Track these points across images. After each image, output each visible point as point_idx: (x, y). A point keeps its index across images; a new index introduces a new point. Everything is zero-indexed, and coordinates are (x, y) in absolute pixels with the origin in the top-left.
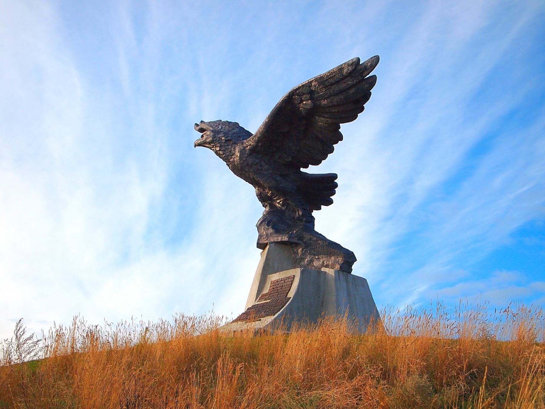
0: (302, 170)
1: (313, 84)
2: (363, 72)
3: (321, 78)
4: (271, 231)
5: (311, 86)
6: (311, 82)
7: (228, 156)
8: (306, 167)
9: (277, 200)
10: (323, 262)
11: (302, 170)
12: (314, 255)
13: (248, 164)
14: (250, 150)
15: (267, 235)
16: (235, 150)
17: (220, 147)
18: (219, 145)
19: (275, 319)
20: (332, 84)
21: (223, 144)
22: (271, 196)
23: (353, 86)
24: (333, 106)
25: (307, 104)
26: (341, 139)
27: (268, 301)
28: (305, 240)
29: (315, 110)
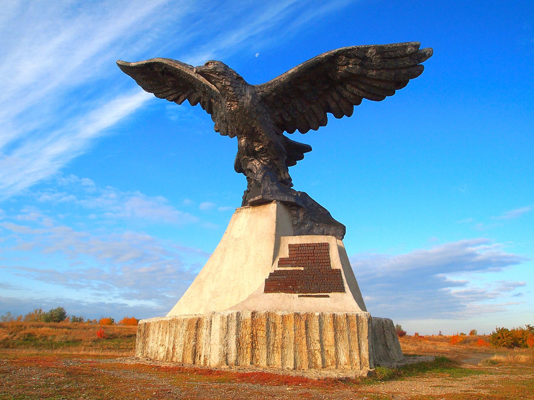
0: (285, 133)
1: (370, 51)
2: (421, 57)
3: (382, 48)
4: (275, 188)
5: (367, 52)
6: (368, 48)
7: (237, 95)
8: (291, 132)
9: (264, 156)
10: (323, 231)
11: (285, 133)
12: (315, 222)
13: (257, 110)
14: (261, 96)
15: (272, 191)
16: (245, 91)
17: (231, 82)
18: (230, 80)
19: (329, 293)
20: (390, 58)
21: (233, 80)
22: (259, 152)
23: (408, 67)
24: (380, 80)
25: (351, 67)
26: (349, 116)
27: (302, 269)
28: (308, 205)
29: (350, 78)
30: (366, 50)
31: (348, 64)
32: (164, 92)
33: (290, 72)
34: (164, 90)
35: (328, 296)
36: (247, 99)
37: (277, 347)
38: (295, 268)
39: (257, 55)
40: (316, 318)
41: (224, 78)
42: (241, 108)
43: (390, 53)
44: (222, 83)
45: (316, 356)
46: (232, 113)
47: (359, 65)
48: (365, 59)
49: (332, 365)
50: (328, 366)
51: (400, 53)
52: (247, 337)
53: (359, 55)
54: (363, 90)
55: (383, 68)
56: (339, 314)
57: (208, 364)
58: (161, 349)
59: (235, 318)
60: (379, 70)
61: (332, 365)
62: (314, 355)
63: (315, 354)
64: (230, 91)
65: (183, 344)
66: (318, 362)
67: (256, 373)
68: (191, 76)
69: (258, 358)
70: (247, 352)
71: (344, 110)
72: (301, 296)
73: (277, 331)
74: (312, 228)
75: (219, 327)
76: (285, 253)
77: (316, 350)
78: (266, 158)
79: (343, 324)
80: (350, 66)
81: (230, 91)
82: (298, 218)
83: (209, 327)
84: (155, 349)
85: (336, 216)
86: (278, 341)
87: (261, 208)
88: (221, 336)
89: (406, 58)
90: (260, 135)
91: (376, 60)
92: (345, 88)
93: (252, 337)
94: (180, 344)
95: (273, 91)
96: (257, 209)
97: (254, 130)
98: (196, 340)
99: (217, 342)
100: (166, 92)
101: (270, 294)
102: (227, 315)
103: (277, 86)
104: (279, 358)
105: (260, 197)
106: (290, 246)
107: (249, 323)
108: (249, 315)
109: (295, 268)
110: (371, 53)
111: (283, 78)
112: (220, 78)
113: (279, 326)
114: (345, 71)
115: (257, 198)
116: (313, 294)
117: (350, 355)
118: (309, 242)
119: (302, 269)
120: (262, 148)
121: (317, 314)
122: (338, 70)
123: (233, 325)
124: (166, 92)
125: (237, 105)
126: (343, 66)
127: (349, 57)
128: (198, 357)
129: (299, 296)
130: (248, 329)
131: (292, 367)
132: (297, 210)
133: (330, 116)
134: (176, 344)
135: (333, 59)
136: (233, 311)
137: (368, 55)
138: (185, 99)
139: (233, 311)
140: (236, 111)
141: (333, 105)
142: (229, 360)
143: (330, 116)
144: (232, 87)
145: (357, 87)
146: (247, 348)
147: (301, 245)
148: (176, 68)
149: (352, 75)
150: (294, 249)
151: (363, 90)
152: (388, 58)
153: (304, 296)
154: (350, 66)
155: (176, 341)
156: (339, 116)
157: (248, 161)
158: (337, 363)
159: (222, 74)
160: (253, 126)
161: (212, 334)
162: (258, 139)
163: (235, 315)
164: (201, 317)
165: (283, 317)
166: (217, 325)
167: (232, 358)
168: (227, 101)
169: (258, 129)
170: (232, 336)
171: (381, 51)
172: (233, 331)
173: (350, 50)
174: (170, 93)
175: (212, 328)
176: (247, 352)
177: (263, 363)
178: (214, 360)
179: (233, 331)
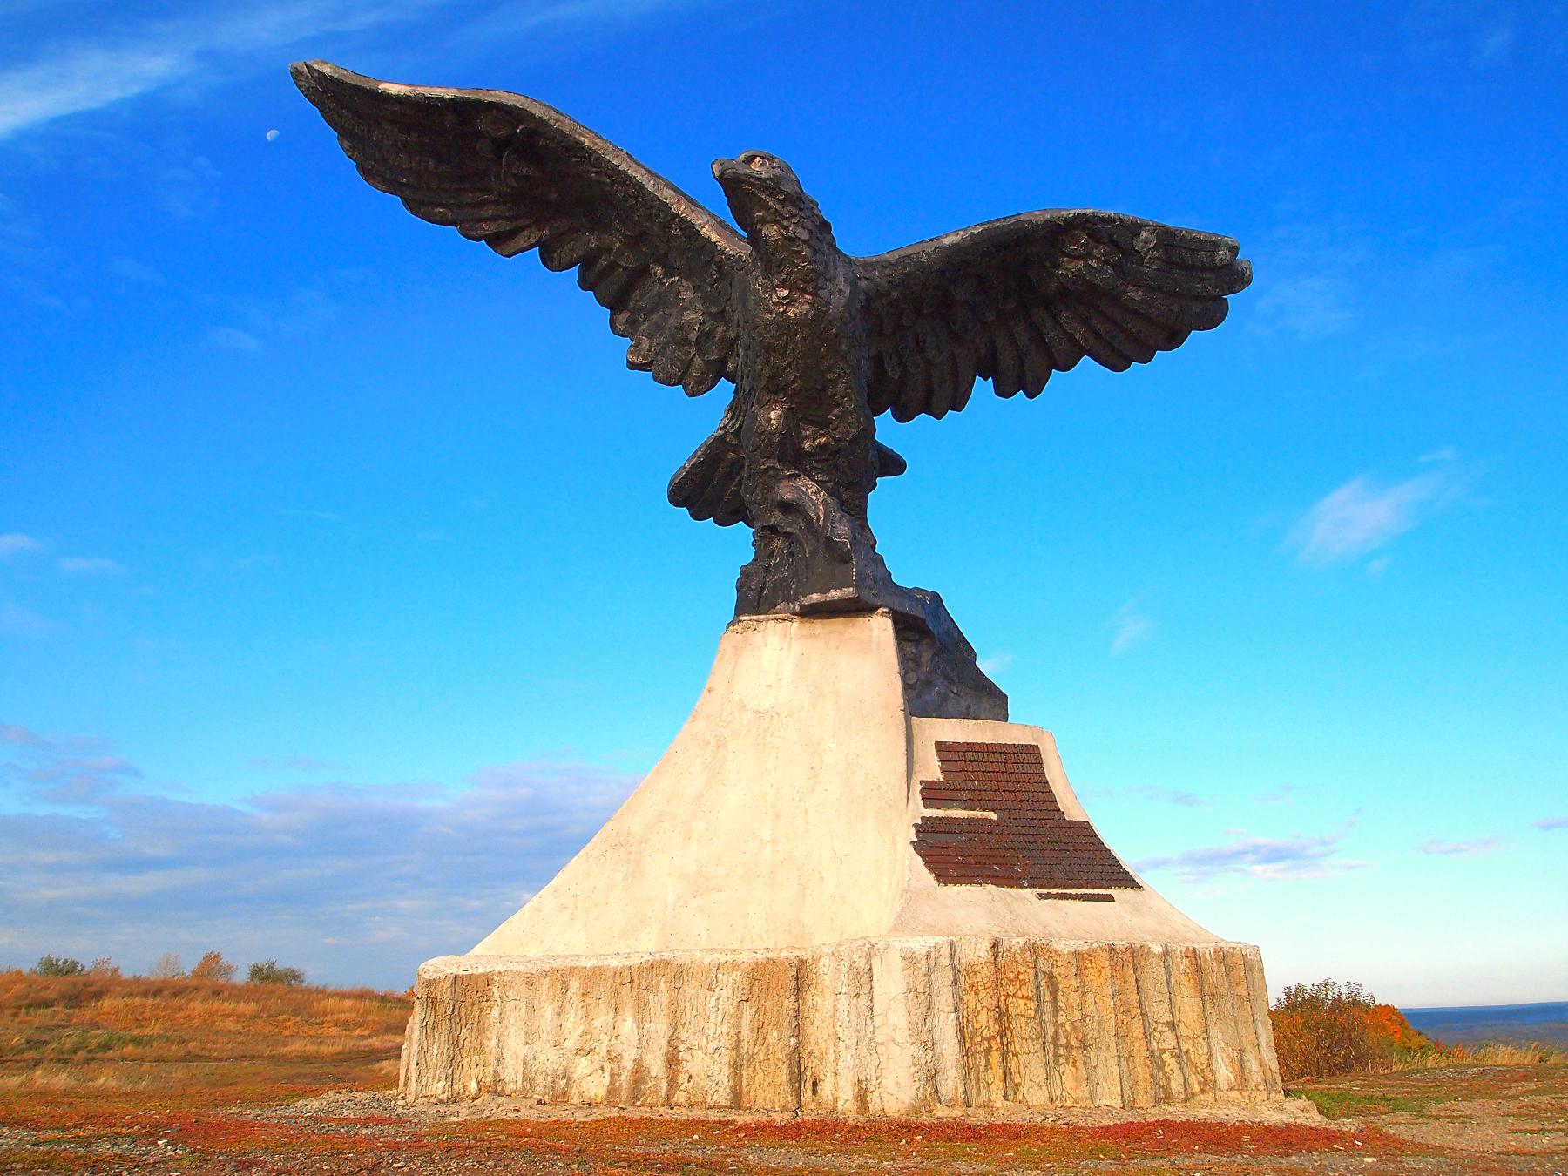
1: (1144, 234)
9: (822, 471)
22: (810, 455)
25: (1091, 265)
26: (1031, 395)
27: (993, 816)
29: (1084, 295)
30: (1135, 228)
31: (1089, 255)
32: (459, 206)
33: (946, 241)
34: (468, 197)
35: (1110, 898)
36: (838, 296)
37: (1068, 1046)
38: (972, 814)
39: (271, 135)
40: (1155, 960)
41: (793, 216)
42: (820, 316)
43: (1185, 253)
44: (786, 228)
45: (1167, 1069)
46: (783, 324)
47: (1114, 266)
48: (1130, 252)
49: (1203, 1091)
50: (1193, 1094)
51: (1204, 257)
52: (983, 1017)
53: (1112, 235)
54: (1097, 334)
55: (1160, 288)
56: (1201, 948)
57: (875, 1107)
58: (583, 1066)
59: (947, 961)
60: (1152, 289)
61: (1203, 1091)
62: (1161, 1065)
63: (1164, 1062)
64: (804, 259)
65: (726, 1042)
66: (1173, 1084)
67: (660, 1123)
68: (631, 178)
69: (1017, 1080)
70: (988, 1063)
71: (1021, 379)
72: (1047, 896)
73: (1060, 997)
74: (945, 698)
75: (903, 989)
76: (932, 769)
77: (1163, 1051)
78: (826, 478)
79: (1215, 976)
80: (1093, 263)
81: (804, 259)
82: (918, 664)
83: (866, 989)
84: (548, 1059)
85: (986, 665)
86: (1068, 1027)
87: (838, 624)
88: (914, 1018)
89: (1209, 275)
90: (838, 405)
91: (1151, 264)
92: (1055, 317)
93: (998, 1020)
94: (715, 1044)
95: (894, 286)
96: (819, 626)
97: (823, 389)
98: (798, 1030)
99: (902, 1034)
100: (472, 205)
101: (964, 887)
102: (924, 951)
103: (908, 275)
104: (1076, 1079)
105: (849, 592)
106: (941, 748)
107: (985, 975)
108: (982, 951)
109: (972, 814)
110: (1146, 242)
111: (928, 254)
112: (784, 211)
113: (1067, 983)
114: (1078, 275)
115: (834, 594)
116: (1073, 892)
117: (1242, 1062)
118: (988, 739)
119: (993, 816)
120: (825, 444)
121: (1157, 949)
122: (1057, 266)
123: (943, 979)
124: (472, 205)
125: (811, 304)
126: (1075, 258)
127: (1095, 237)
128: (809, 1085)
129: (1042, 897)
130: (982, 994)
131: (1117, 1103)
132: (917, 642)
133: (983, 387)
134: (682, 1047)
135: (1059, 232)
136: (938, 939)
137: (1138, 245)
138: (531, 247)
139: (938, 939)
140: (801, 322)
141: (1007, 358)
142: (942, 1089)
143: (983, 387)
144: (810, 246)
145: (1085, 322)
146: (988, 1051)
147: (970, 748)
148: (578, 142)
149: (1091, 286)
150: (952, 757)
151: (1097, 334)
152: (1177, 264)
153: (1055, 896)
154: (1093, 263)
155: (683, 1036)
156: (1003, 391)
157: (779, 478)
158: (1209, 1084)
159: (793, 204)
160: (829, 376)
161: (876, 1010)
162: (825, 416)
163: (945, 951)
164: (807, 955)
165: (1077, 955)
166: (890, 984)
167: (950, 1082)
168: (783, 285)
169: (841, 387)
170: (943, 1016)
171: (1168, 238)
172: (944, 1001)
173: (1102, 220)
174: (489, 212)
175: (876, 991)
176: (988, 1063)
177: (1034, 1095)
178: (896, 1094)
179: (942, 999)
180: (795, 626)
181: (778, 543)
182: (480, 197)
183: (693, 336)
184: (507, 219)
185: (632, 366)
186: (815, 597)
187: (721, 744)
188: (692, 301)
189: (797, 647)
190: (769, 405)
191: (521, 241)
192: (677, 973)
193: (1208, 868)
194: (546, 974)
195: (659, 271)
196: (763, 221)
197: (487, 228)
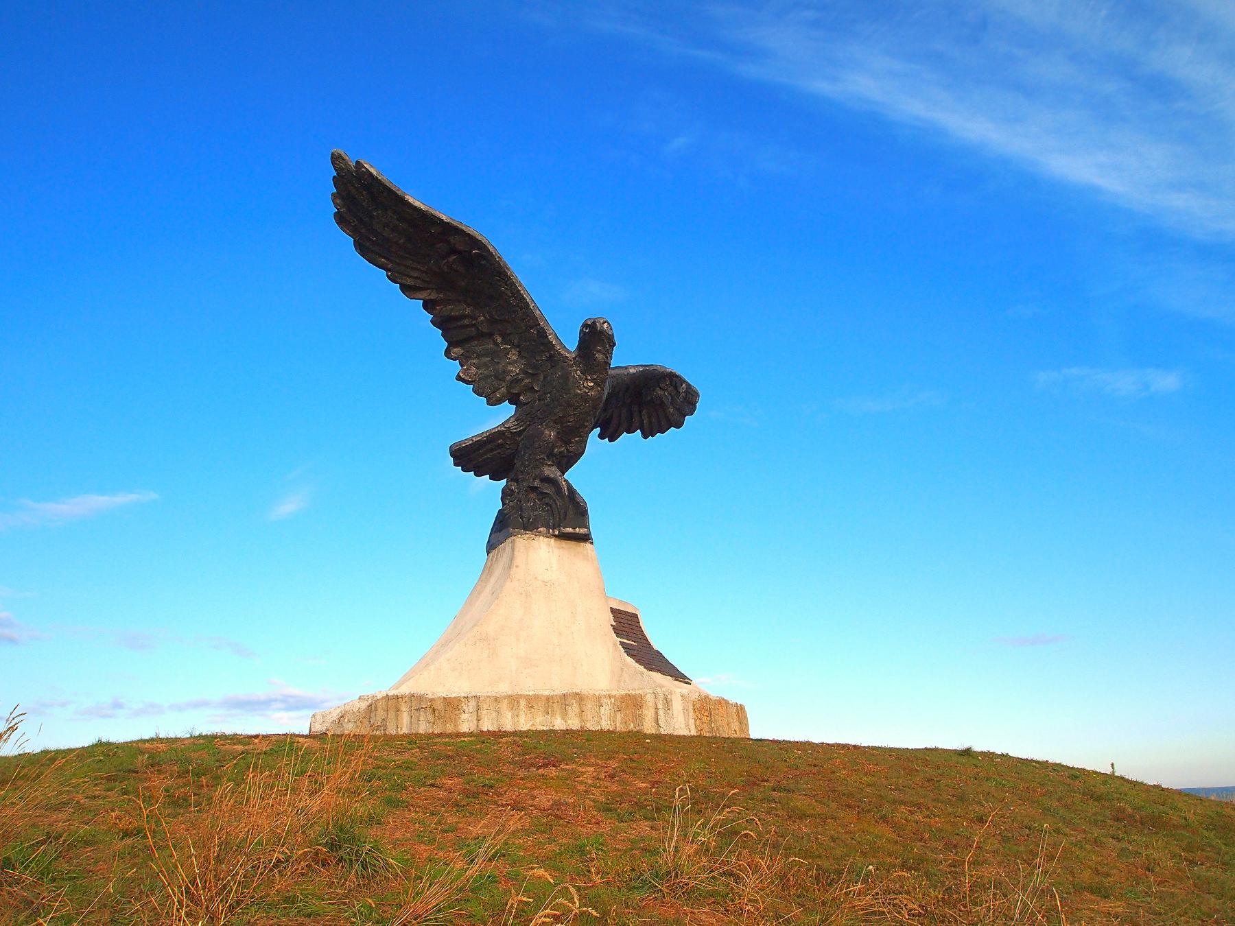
26: (610, 441)
30: (682, 381)
34: (409, 263)
46: (584, 398)
87: (572, 544)
96: (564, 544)
100: (407, 267)
124: (407, 267)
145: (649, 417)
180: (552, 540)
181: (533, 496)
182: (415, 265)
183: (508, 378)
184: (424, 281)
185: (459, 378)
186: (570, 530)
187: (528, 595)
188: (515, 361)
189: (556, 552)
190: (551, 428)
191: (418, 295)
192: (580, 697)
193: (238, 711)
194: (505, 697)
195: (499, 340)
196: (599, 351)
197: (409, 282)
